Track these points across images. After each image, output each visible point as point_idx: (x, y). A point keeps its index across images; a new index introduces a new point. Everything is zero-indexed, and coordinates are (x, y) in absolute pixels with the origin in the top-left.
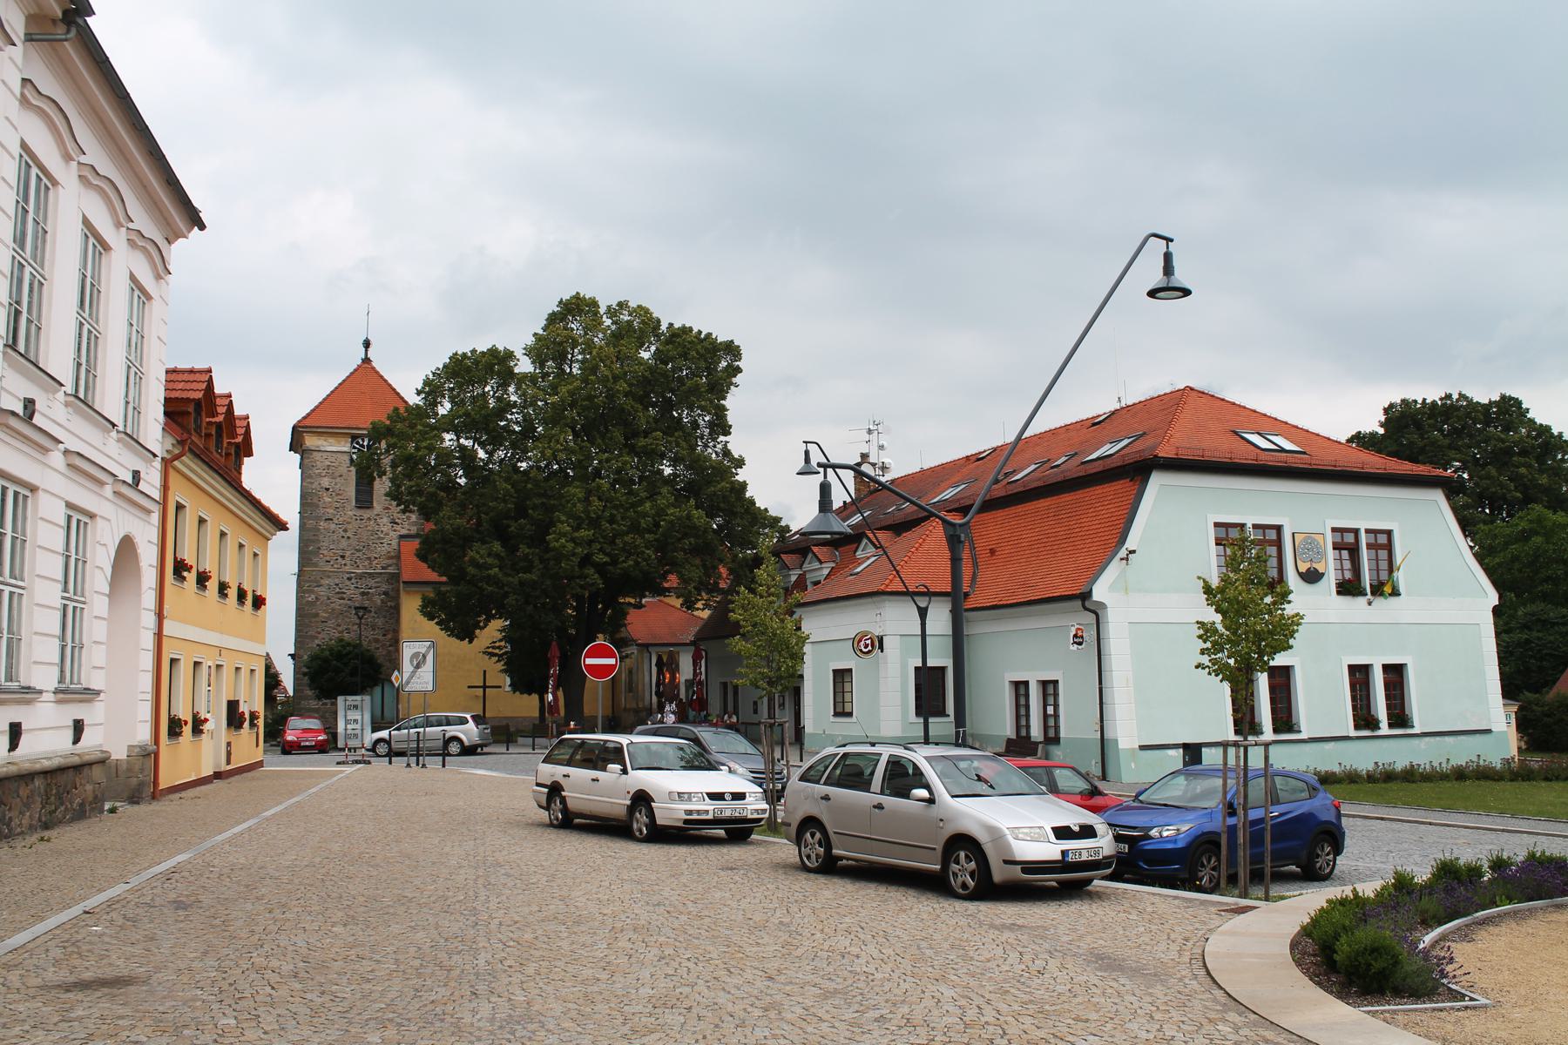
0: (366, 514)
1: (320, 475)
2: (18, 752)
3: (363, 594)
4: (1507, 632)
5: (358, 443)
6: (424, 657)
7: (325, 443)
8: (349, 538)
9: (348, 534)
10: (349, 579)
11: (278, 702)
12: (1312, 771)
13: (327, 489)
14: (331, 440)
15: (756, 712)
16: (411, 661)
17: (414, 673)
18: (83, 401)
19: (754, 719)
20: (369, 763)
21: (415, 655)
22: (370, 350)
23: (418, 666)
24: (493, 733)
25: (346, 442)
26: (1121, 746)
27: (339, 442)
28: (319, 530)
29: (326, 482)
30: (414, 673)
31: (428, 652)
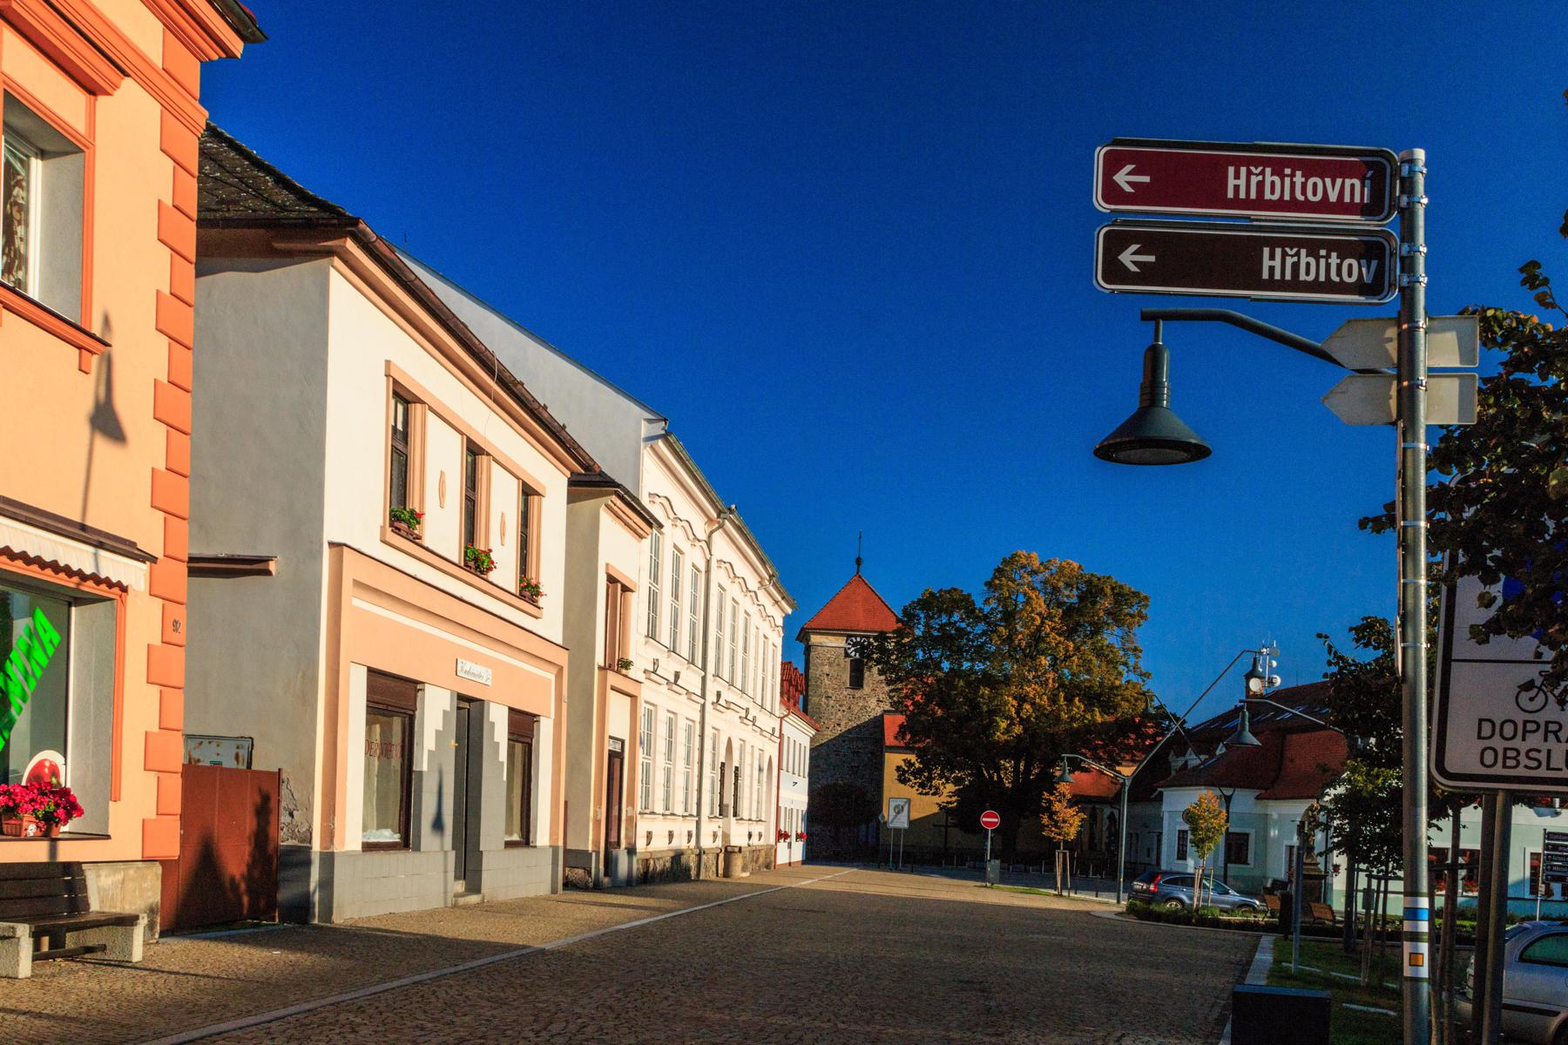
0: (858, 694)
1: (822, 664)
2: (672, 844)
3: (854, 752)
4: (812, 844)
5: (852, 641)
6: (902, 807)
7: (826, 641)
8: (844, 711)
9: (844, 708)
10: (844, 741)
11: (1027, 867)
12: (720, 822)
13: (828, 675)
14: (830, 638)
15: (1148, 856)
16: (895, 810)
17: (895, 817)
18: (731, 684)
19: (1146, 860)
20: (1363, 619)
21: (897, 807)
22: (861, 568)
23: (898, 813)
24: (1128, 908)
25: (842, 640)
26: (1335, 887)
27: (838, 640)
28: (821, 704)
29: (826, 669)
30: (895, 817)
31: (905, 805)
